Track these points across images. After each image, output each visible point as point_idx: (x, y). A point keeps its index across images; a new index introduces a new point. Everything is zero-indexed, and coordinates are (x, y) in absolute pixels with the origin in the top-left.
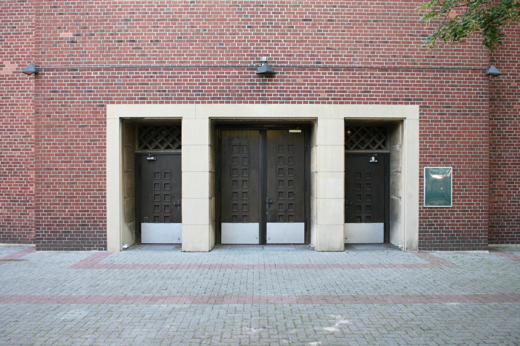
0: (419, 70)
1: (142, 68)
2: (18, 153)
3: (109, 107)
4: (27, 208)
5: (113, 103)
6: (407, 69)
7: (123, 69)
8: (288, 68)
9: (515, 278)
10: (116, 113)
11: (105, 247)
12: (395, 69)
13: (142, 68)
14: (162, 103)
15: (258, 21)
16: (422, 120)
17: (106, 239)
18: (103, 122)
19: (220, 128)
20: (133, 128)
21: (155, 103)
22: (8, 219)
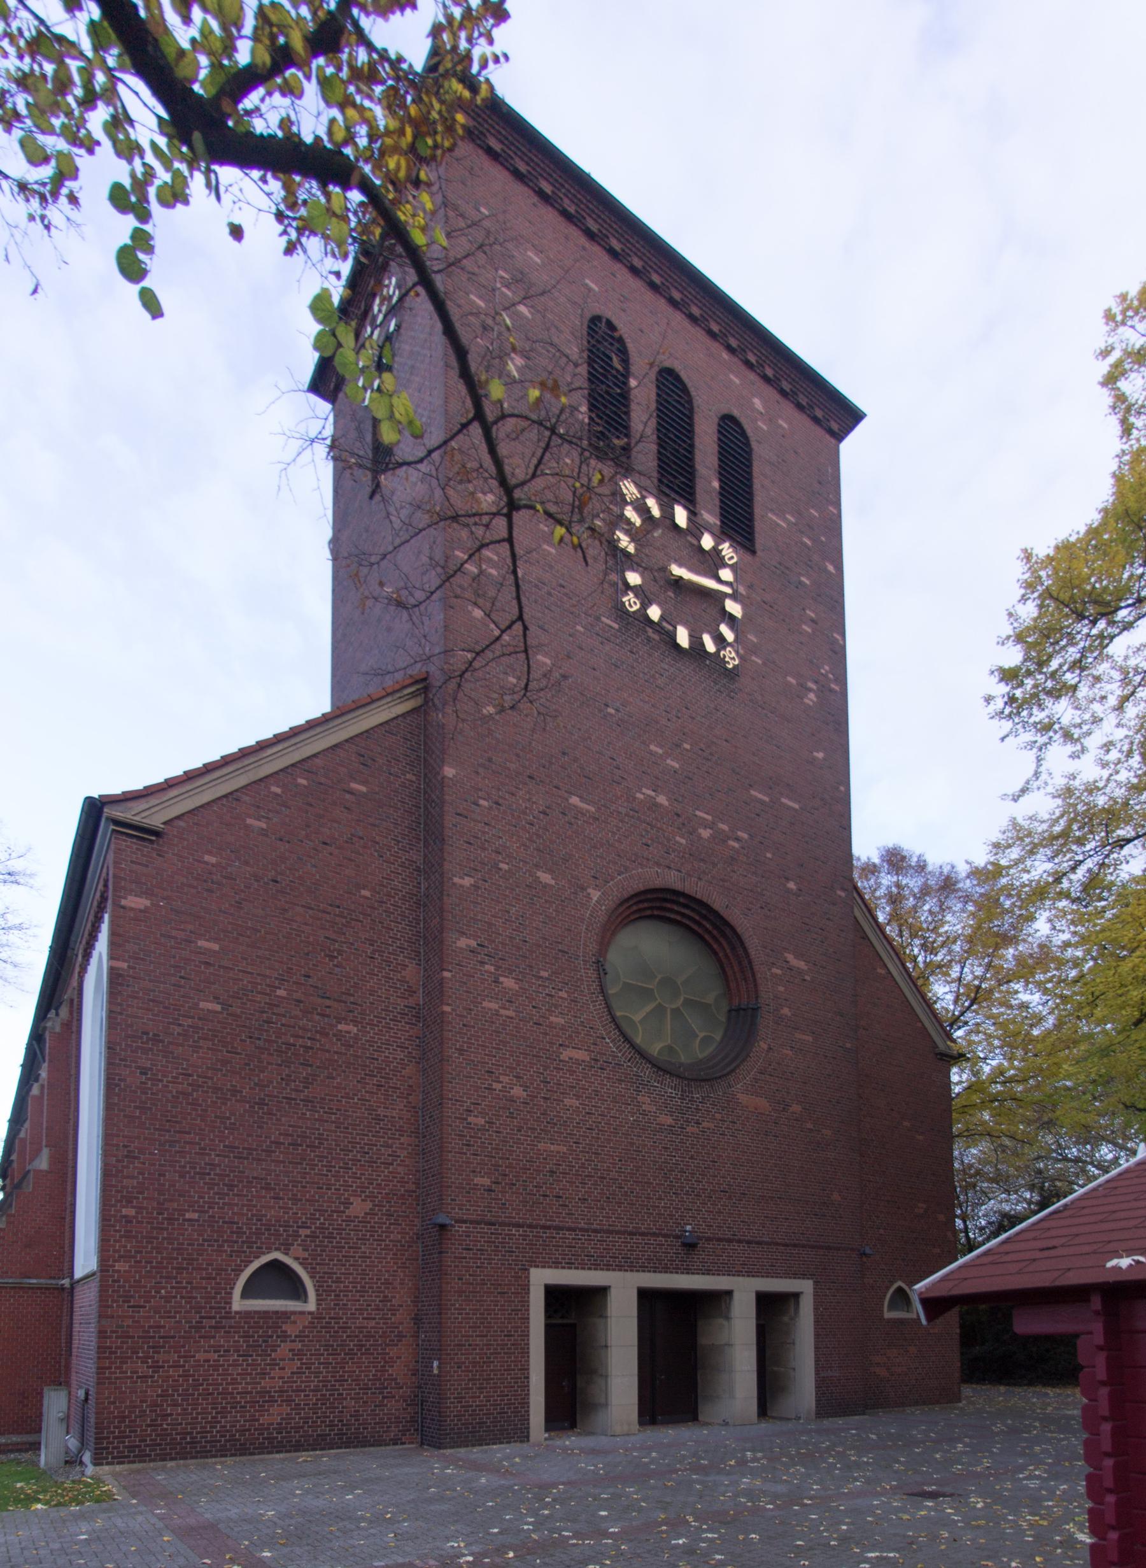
0: (813, 1247)
1: (570, 1229)
2: (372, 1323)
3: (533, 1271)
4: (384, 1397)
5: (537, 1266)
6: (804, 1246)
7: (549, 1228)
8: (709, 1239)
9: (1065, 865)
10: (541, 1278)
11: (528, 1437)
12: (795, 1246)
13: (570, 1229)
14: (590, 1269)
15: (682, 1188)
16: (816, 1295)
17: (528, 1428)
18: (526, 1288)
19: (645, 1295)
20: (556, 1296)
21: (583, 1269)
22: (356, 1415)
